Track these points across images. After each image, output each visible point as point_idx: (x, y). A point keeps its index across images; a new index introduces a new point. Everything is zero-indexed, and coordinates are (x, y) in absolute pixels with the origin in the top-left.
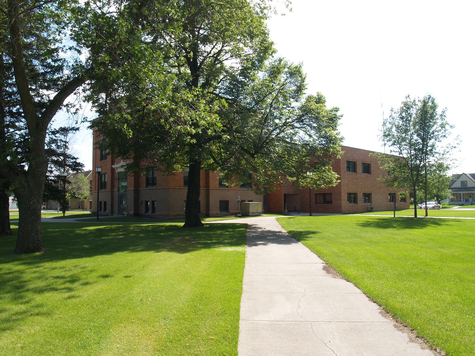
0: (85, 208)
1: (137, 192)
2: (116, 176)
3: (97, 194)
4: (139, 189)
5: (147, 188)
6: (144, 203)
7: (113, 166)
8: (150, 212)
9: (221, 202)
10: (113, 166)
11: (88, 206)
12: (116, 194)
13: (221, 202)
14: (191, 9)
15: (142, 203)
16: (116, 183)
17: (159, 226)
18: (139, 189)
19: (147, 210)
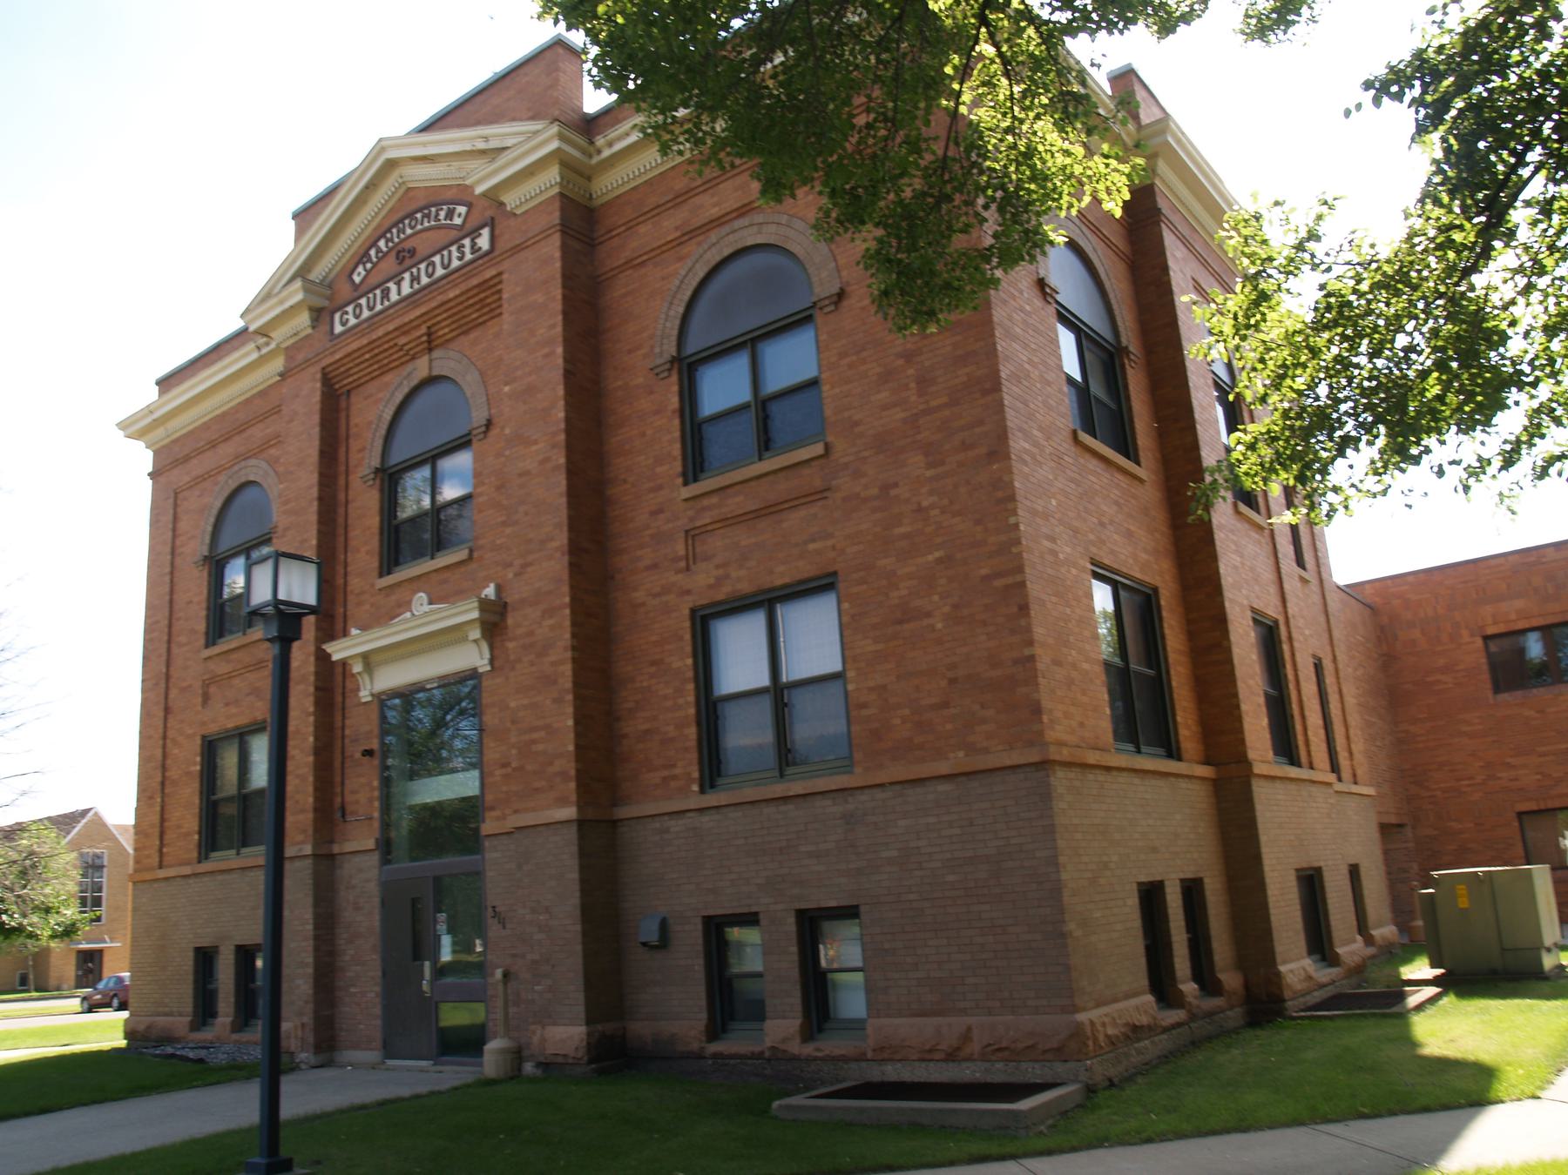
0: (53, 982)
1: (602, 840)
2: (361, 727)
3: (260, 880)
4: (623, 812)
5: (711, 799)
6: (690, 939)
7: (338, 650)
8: (781, 1028)
9: (198, 950)
10: (338, 650)
11: (70, 970)
12: (363, 876)
13: (198, 950)
14: (1471, 375)
15: (664, 942)
16: (361, 788)
17: (954, 1111)
18: (623, 812)
19: (728, 1001)
